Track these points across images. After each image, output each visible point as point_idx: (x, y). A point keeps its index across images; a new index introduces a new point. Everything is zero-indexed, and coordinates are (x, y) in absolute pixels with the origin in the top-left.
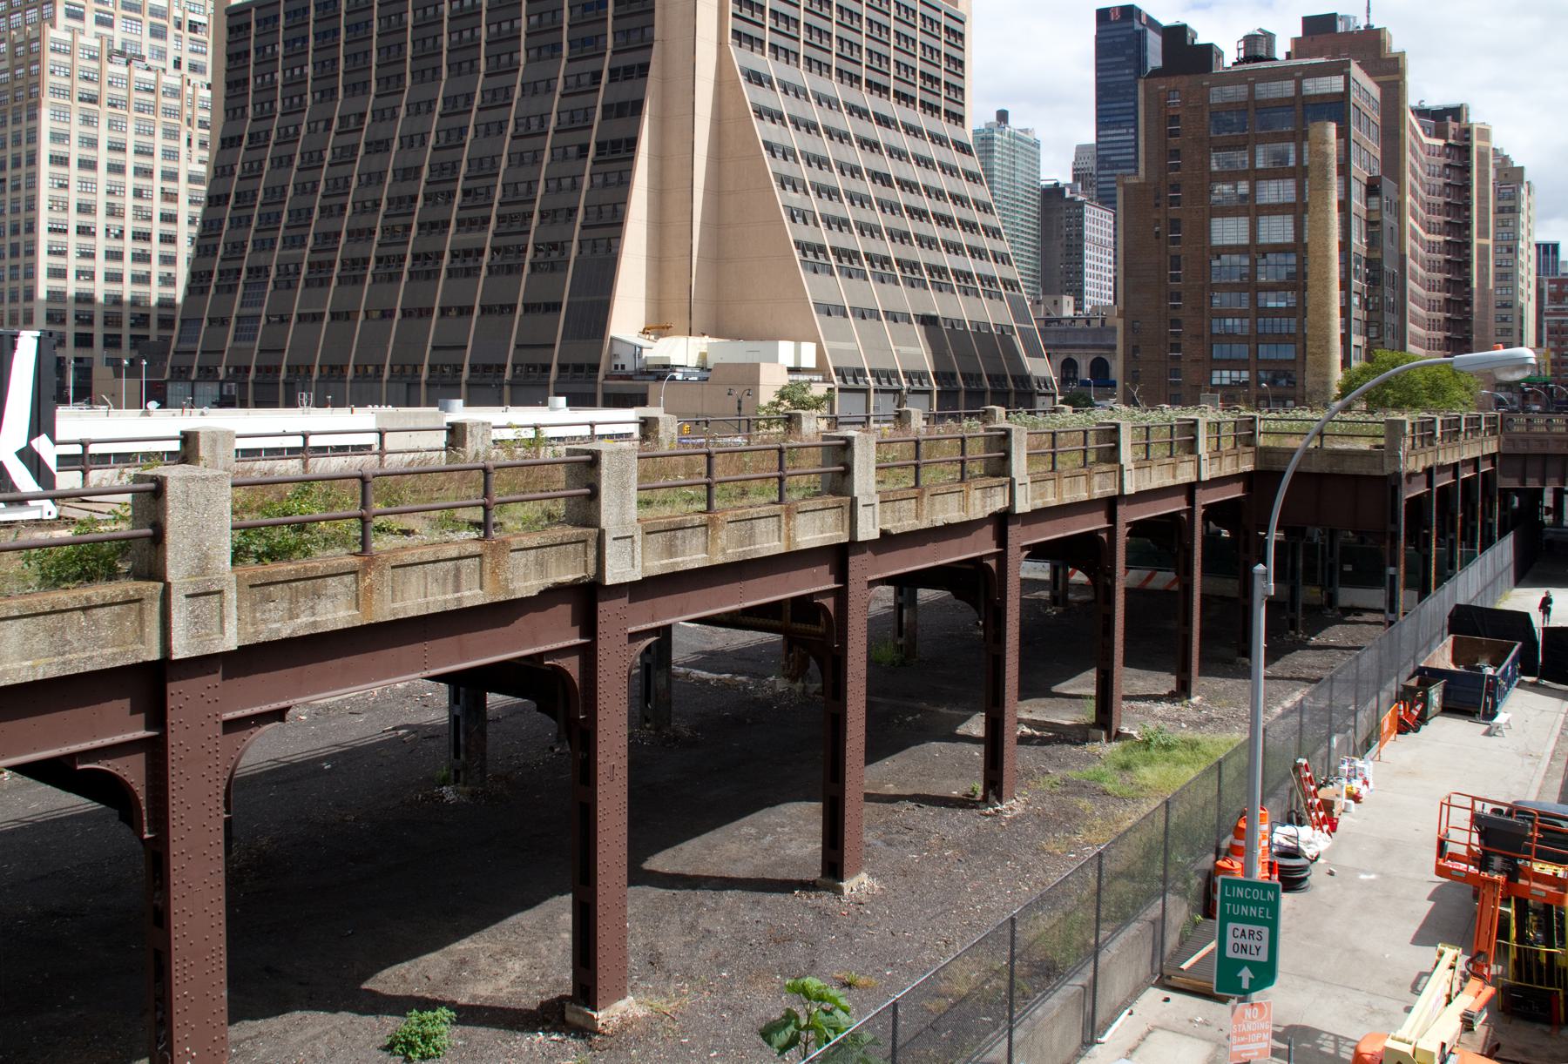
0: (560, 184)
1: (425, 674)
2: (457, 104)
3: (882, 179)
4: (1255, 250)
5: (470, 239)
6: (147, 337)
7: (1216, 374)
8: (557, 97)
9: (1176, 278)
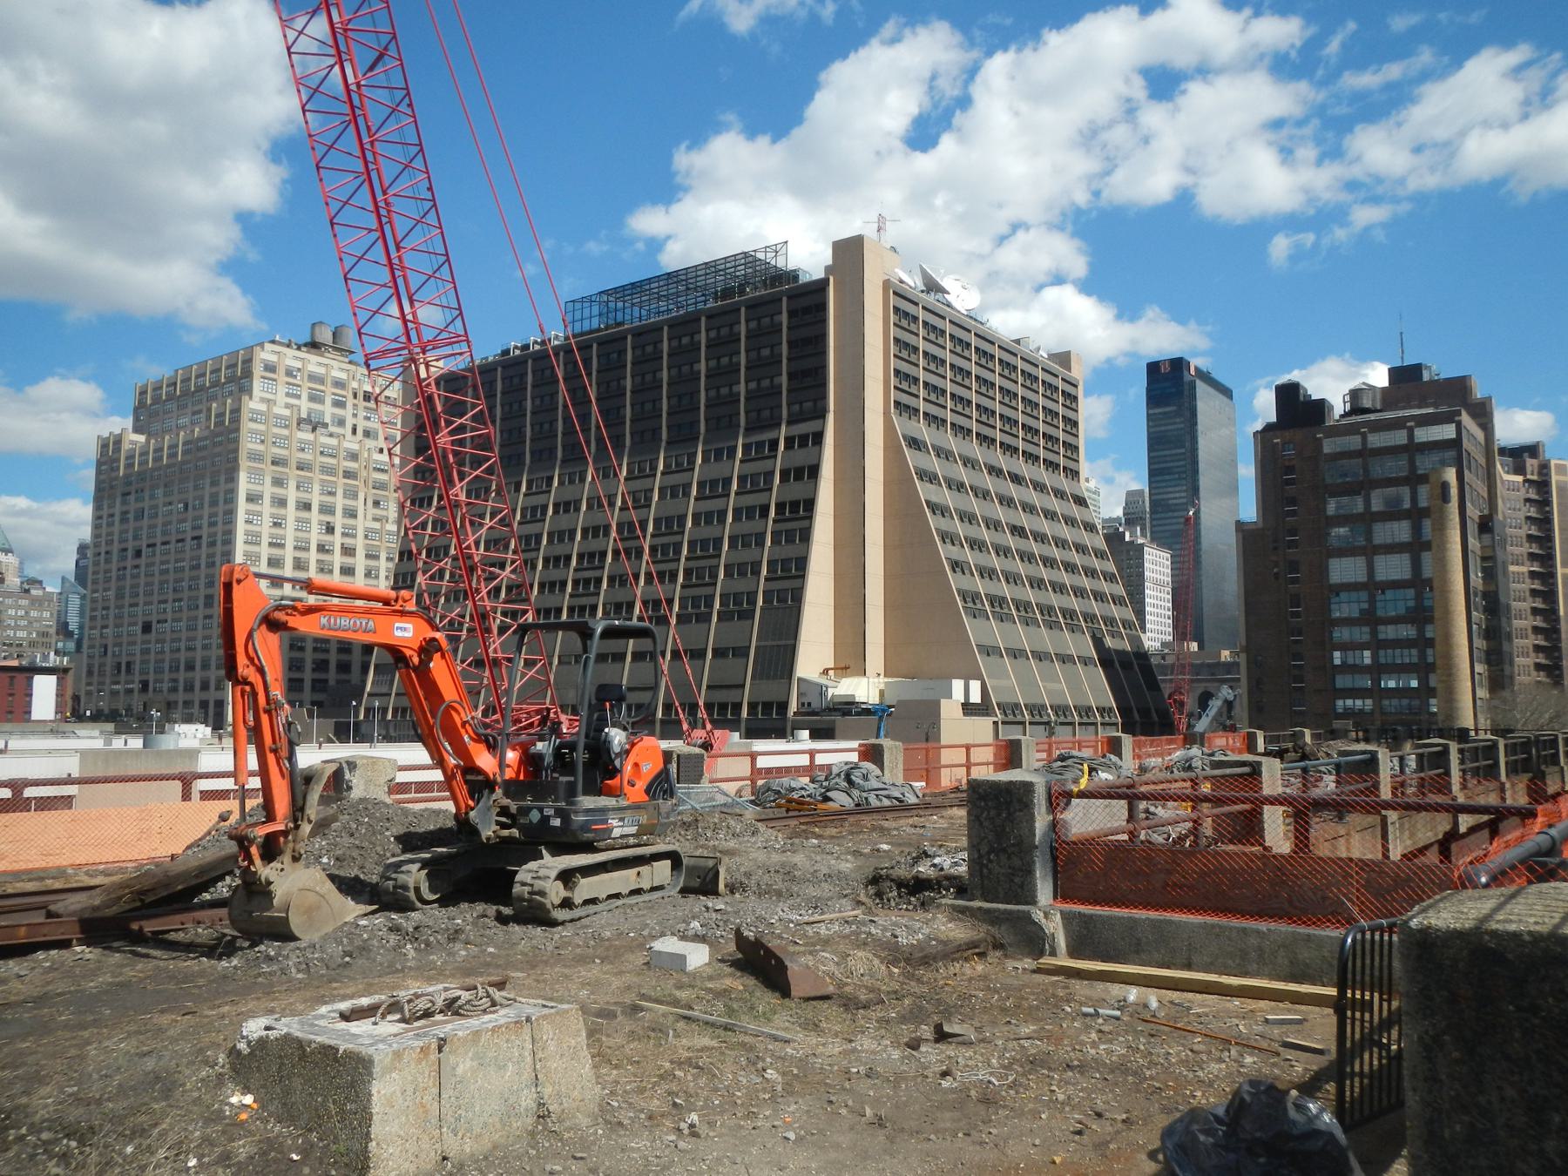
1: (345, 1006)
3: (1018, 531)
4: (1373, 587)
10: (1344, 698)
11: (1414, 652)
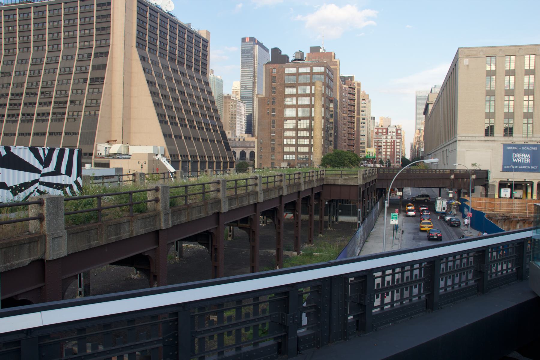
0: (77, 92)
2: (38, 62)
5: (44, 109)
7: (285, 156)
8: (75, 61)
9: (273, 127)
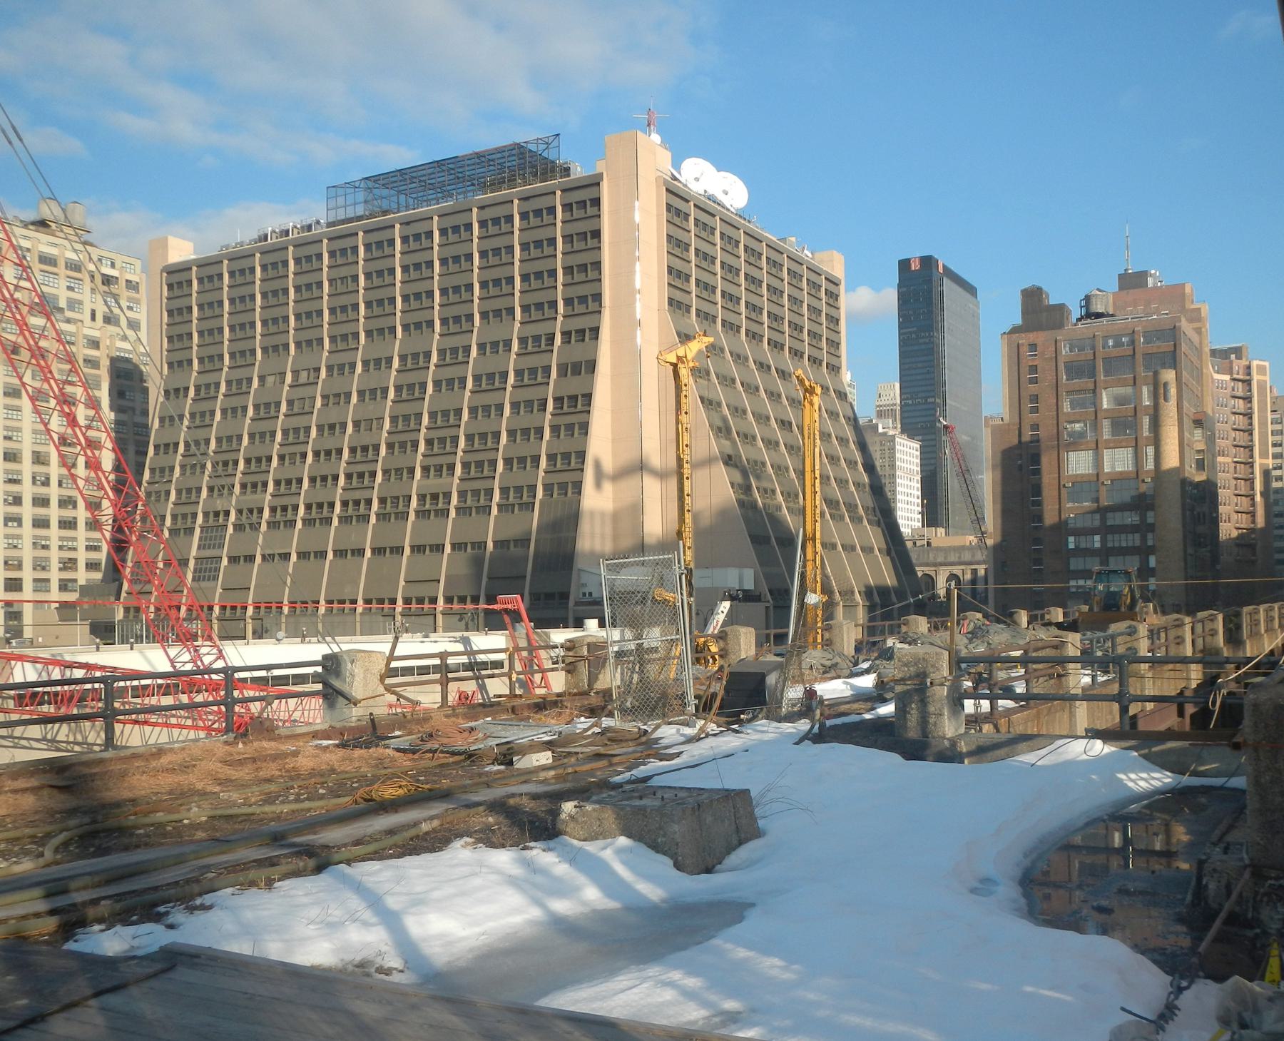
6: (75, 581)
10: (1076, 579)
11: (1137, 536)
